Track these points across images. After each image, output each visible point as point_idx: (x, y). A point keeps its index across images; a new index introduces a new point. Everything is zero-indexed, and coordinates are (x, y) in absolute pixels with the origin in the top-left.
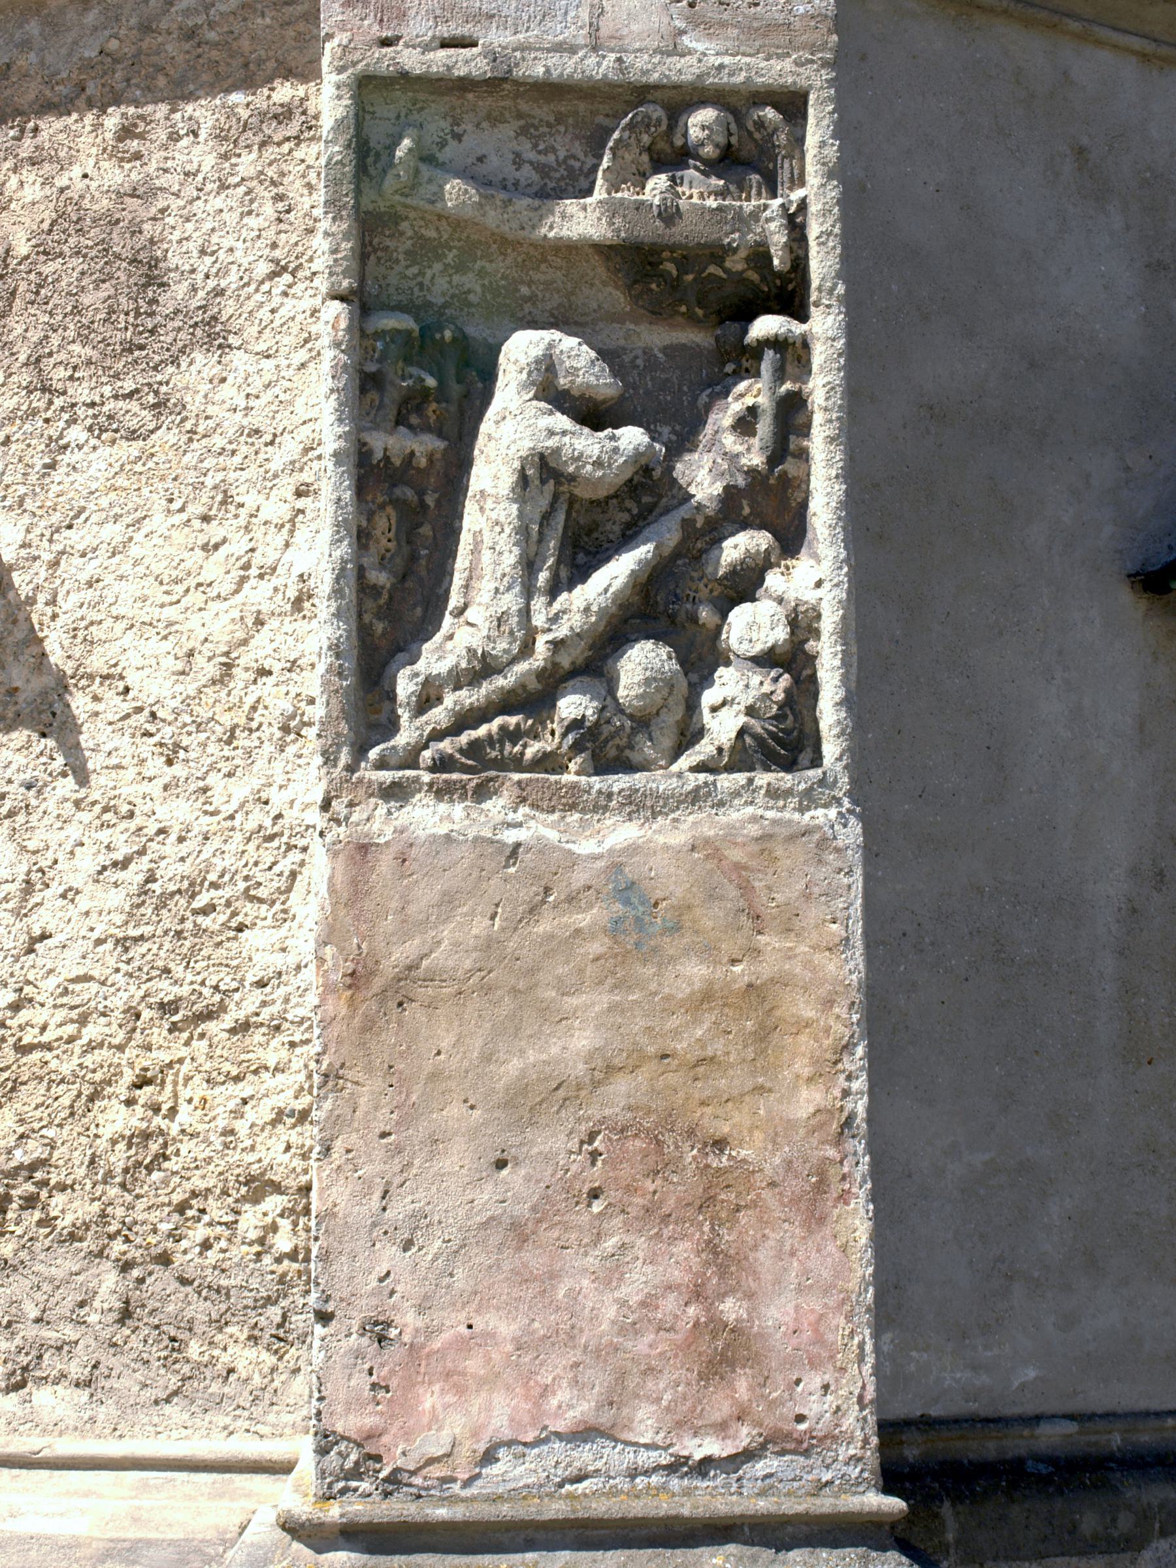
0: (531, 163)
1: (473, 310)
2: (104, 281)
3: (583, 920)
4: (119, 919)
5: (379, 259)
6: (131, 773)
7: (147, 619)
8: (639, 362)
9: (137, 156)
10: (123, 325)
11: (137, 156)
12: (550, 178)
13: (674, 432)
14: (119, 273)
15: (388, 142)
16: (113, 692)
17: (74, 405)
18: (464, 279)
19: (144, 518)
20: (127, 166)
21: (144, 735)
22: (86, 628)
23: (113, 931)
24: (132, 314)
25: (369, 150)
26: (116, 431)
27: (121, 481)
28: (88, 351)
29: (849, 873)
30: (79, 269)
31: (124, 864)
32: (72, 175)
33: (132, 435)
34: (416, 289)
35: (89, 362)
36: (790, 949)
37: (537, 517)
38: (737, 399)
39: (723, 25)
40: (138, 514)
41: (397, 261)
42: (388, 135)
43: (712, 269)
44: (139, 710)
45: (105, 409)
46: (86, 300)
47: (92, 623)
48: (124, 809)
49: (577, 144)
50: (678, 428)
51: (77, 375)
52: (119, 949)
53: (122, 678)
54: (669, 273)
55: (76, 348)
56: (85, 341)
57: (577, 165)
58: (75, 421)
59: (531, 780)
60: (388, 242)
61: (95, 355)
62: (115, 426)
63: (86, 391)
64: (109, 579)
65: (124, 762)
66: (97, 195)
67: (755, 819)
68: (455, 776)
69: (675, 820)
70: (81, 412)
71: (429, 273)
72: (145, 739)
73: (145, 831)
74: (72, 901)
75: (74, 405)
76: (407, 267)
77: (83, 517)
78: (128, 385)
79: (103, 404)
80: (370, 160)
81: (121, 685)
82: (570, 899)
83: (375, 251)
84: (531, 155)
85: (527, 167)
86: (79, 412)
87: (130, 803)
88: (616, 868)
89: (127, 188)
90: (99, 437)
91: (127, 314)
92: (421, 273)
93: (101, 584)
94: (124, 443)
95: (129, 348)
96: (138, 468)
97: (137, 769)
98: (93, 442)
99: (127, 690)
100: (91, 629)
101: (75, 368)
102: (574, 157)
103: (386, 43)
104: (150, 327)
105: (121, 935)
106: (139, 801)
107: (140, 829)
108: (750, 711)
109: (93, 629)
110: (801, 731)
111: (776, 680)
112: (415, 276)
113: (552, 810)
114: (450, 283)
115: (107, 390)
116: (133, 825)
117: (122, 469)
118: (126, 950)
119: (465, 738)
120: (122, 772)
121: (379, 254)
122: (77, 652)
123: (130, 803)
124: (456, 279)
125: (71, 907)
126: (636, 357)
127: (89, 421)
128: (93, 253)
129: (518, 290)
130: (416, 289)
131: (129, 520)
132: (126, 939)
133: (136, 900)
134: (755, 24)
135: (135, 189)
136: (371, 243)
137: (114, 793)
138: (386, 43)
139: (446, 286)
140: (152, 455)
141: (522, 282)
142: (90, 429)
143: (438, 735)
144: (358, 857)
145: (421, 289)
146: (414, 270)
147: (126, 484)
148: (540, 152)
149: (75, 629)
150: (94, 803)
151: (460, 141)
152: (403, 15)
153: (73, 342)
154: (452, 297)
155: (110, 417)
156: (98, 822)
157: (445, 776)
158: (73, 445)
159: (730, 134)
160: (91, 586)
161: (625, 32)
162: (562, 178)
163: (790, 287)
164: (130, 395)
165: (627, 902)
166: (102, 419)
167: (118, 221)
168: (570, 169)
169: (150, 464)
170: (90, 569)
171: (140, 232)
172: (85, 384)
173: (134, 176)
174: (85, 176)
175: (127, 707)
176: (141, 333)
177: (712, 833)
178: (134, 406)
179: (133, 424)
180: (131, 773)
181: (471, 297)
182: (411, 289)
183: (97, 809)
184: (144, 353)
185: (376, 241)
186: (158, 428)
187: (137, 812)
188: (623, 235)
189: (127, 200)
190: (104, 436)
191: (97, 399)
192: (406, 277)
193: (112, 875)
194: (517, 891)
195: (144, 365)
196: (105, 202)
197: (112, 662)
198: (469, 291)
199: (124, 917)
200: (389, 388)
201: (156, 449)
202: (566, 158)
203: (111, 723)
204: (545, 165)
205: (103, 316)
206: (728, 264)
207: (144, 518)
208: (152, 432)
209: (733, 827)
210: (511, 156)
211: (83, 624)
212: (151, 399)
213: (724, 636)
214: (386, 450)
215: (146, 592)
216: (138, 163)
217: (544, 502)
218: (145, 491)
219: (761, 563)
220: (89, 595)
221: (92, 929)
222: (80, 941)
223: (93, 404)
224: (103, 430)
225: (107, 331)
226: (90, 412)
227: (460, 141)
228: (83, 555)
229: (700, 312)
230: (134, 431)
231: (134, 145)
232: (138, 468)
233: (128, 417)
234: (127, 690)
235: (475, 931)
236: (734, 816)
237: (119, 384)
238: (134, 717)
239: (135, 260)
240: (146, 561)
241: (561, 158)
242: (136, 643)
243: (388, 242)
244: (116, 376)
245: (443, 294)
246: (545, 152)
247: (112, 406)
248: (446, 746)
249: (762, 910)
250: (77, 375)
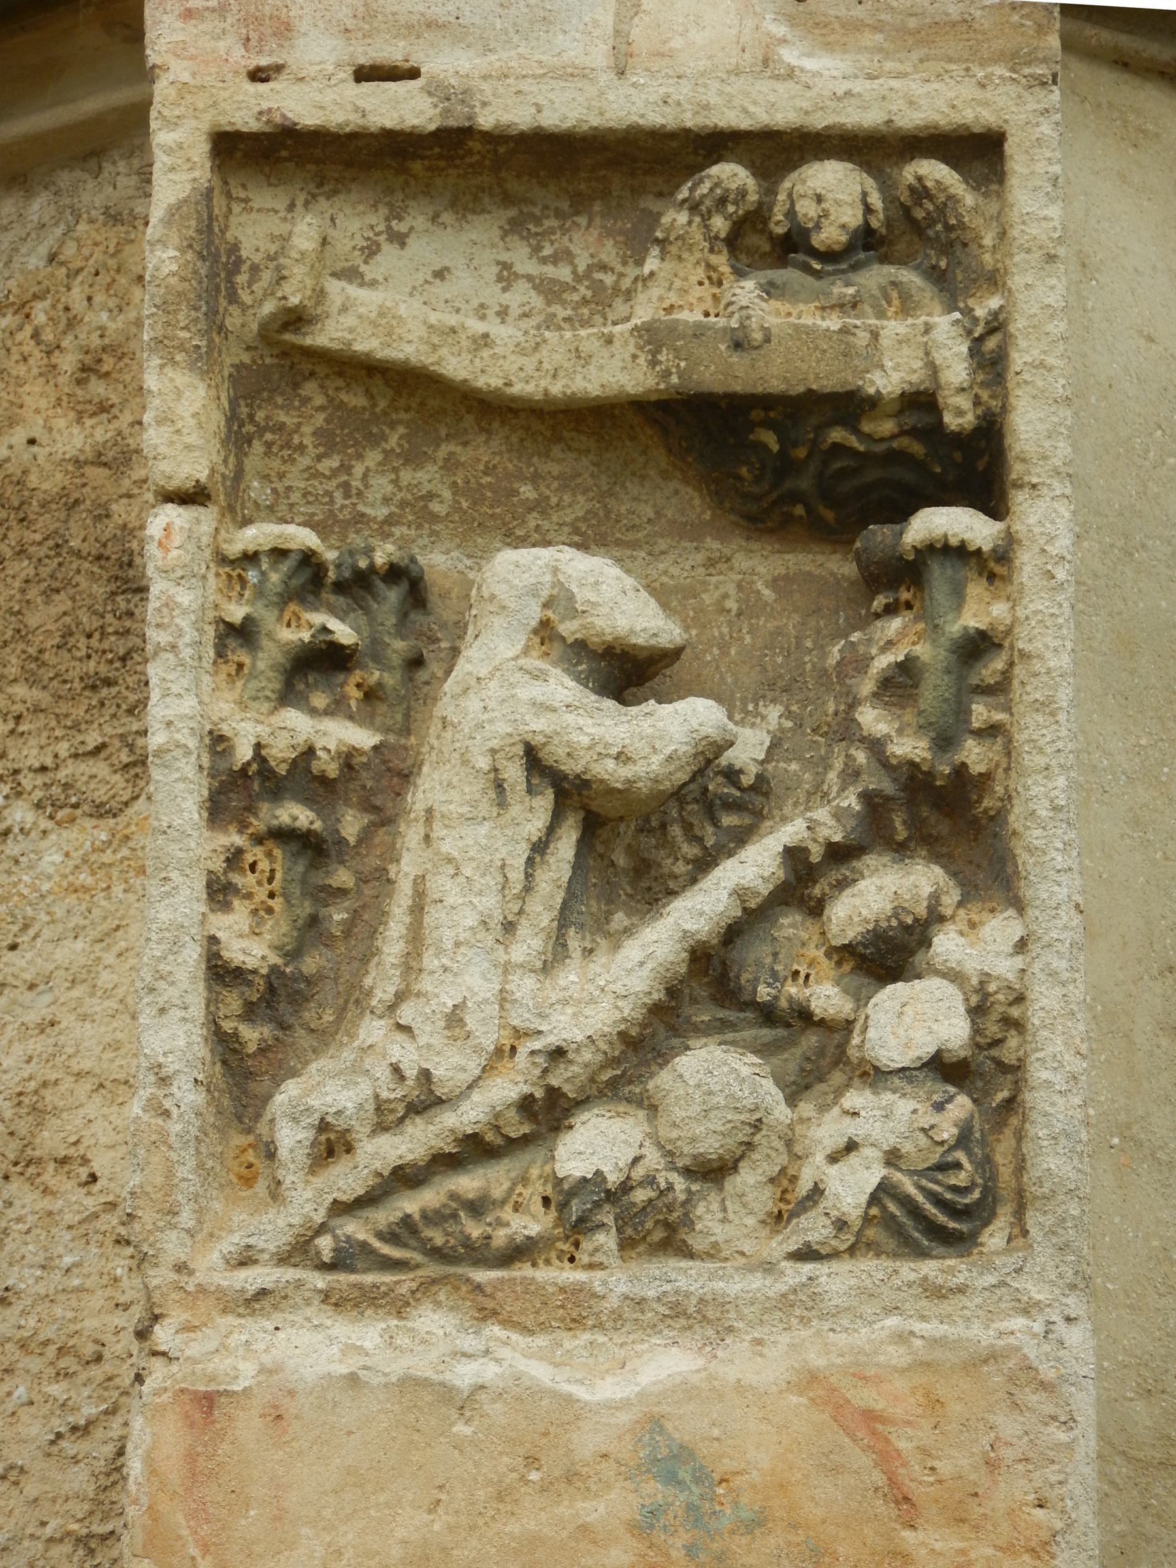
0: (529, 278)
1: (437, 527)
2: (58, 591)
3: (593, 1510)
4: (81, 1509)
5: (269, 445)
6: (97, 1301)
7: (121, 1076)
8: (731, 604)
9: (103, 408)
10: (83, 653)
11: (103, 408)
12: (563, 303)
13: (788, 714)
14: (78, 578)
15: (273, 249)
16: (74, 1182)
17: (16, 772)
18: (423, 476)
19: (118, 928)
20: (89, 422)
21: (118, 1242)
22: (36, 1092)
23: (74, 1527)
24: (97, 635)
25: (239, 261)
26: (76, 806)
27: (84, 878)
28: (36, 694)
29: (1069, 1423)
30: (23, 575)
31: (81, 1431)
32: (14, 440)
33: (101, 811)
34: (338, 495)
35: (37, 710)
36: (963, 1552)
37: (523, 852)
38: (883, 650)
39: (856, 26)
40: (111, 923)
41: (301, 448)
42: (273, 238)
43: (837, 435)
44: (112, 1206)
45: (62, 775)
46: (33, 620)
47: (45, 1084)
48: (89, 1350)
49: (609, 243)
50: (794, 708)
51: (21, 729)
52: (81, 1552)
53: (85, 1161)
54: (765, 447)
55: (20, 690)
56: (32, 681)
57: (609, 279)
58: (19, 794)
59: (502, 1281)
60: (282, 417)
61: (44, 698)
62: (74, 800)
63: (35, 752)
64: (67, 1020)
65: (88, 1284)
66: (48, 467)
67: (902, 1338)
68: (369, 1278)
69: (759, 1342)
70: (27, 781)
71: (359, 469)
72: (117, 1249)
73: (117, 1381)
74: (16, 1483)
75: (16, 772)
76: (319, 458)
77: (31, 932)
78: (93, 739)
79: (57, 767)
80: (242, 279)
81: (84, 1173)
82: (570, 1477)
83: (261, 431)
84: (530, 267)
85: (522, 286)
86: (24, 782)
87: (96, 1341)
88: (655, 1423)
89: (90, 455)
90: (51, 817)
91: (89, 636)
92: (346, 468)
93: (56, 1028)
94: (88, 823)
95: (95, 684)
96: (108, 857)
97: (109, 1292)
98: (45, 824)
99: (93, 1178)
100: (43, 1092)
101: (18, 718)
102: (604, 268)
103: (258, 75)
104: (122, 652)
105: (84, 1531)
106: (107, 1338)
107: (110, 1379)
108: (893, 1158)
109: (47, 1093)
110: (986, 1190)
111: (939, 1107)
112: (335, 473)
113: (544, 1327)
114: (395, 482)
115: (63, 748)
116: (97, 1372)
117: (85, 861)
118: (91, 1552)
119: (385, 1216)
120: (84, 1295)
121: (269, 436)
122: (22, 1127)
123: (96, 1341)
124: (406, 476)
125: (15, 1492)
126: (725, 596)
127: (38, 794)
128: (42, 551)
129: (515, 492)
130: (338, 495)
131: (94, 934)
132: (90, 1536)
133: (103, 1481)
134: (912, 23)
135: (100, 454)
136: (251, 417)
137: (73, 1327)
138: (258, 75)
139: (390, 488)
140: (127, 838)
141: (522, 478)
142: (39, 806)
143: (341, 1209)
144: (197, 1416)
145: (347, 495)
146: (334, 462)
147: (90, 881)
148: (544, 261)
149: (20, 1094)
150: (46, 1343)
151: (403, 245)
152: (285, 30)
153: (15, 680)
154: (403, 504)
155: (66, 786)
156: (51, 1371)
157: (353, 1278)
158: (16, 830)
159: (868, 210)
160: (42, 1031)
161: (677, 43)
162: (585, 301)
163: (981, 465)
164: (99, 749)
165: (671, 1479)
166: (56, 790)
167: (77, 502)
168: (597, 288)
169: (125, 852)
170: (39, 1007)
171: (108, 516)
172: (33, 742)
173: (100, 435)
174: (32, 442)
175: (91, 1203)
176: (111, 662)
177: (821, 1362)
178: (100, 768)
179: (101, 795)
180: (97, 1301)
181: (436, 507)
182: (328, 493)
183: (51, 1351)
184: (114, 690)
185: (260, 415)
186: (137, 797)
187: (107, 1354)
188: (674, 379)
189: (90, 471)
190: (60, 815)
191: (49, 761)
192: (317, 475)
193: (69, 1446)
194: (477, 1464)
195: (113, 709)
196: (59, 476)
197: (73, 1139)
198: (431, 496)
199: (87, 1507)
200: (265, 642)
201: (133, 828)
202: (590, 268)
203: (70, 1227)
204: (553, 281)
205: (57, 640)
206: (867, 427)
207: (118, 928)
208: (126, 804)
209: (861, 1351)
210: (495, 269)
211: (33, 1085)
212: (125, 758)
213: (856, 1040)
214: (258, 746)
215: (119, 1035)
216: (105, 416)
217: (536, 825)
218: (118, 890)
219: (922, 911)
220: (37, 1045)
221: (43, 1524)
222: (26, 1543)
223: (43, 769)
224: (57, 806)
225: (62, 661)
226: (40, 780)
227: (403, 245)
228: (32, 987)
229: (829, 515)
230: (102, 804)
231: (98, 388)
232: (108, 857)
233: (92, 786)
234: (93, 1178)
235: (400, 1533)
236: (863, 1336)
237: (80, 738)
238: (104, 1217)
239: (99, 558)
240: (120, 991)
241: (581, 269)
242: (105, 1111)
243: (282, 417)
244: (76, 727)
245: (386, 500)
246: (555, 260)
247: (68, 771)
248: (354, 1229)
249: (911, 1487)
250: (21, 729)
